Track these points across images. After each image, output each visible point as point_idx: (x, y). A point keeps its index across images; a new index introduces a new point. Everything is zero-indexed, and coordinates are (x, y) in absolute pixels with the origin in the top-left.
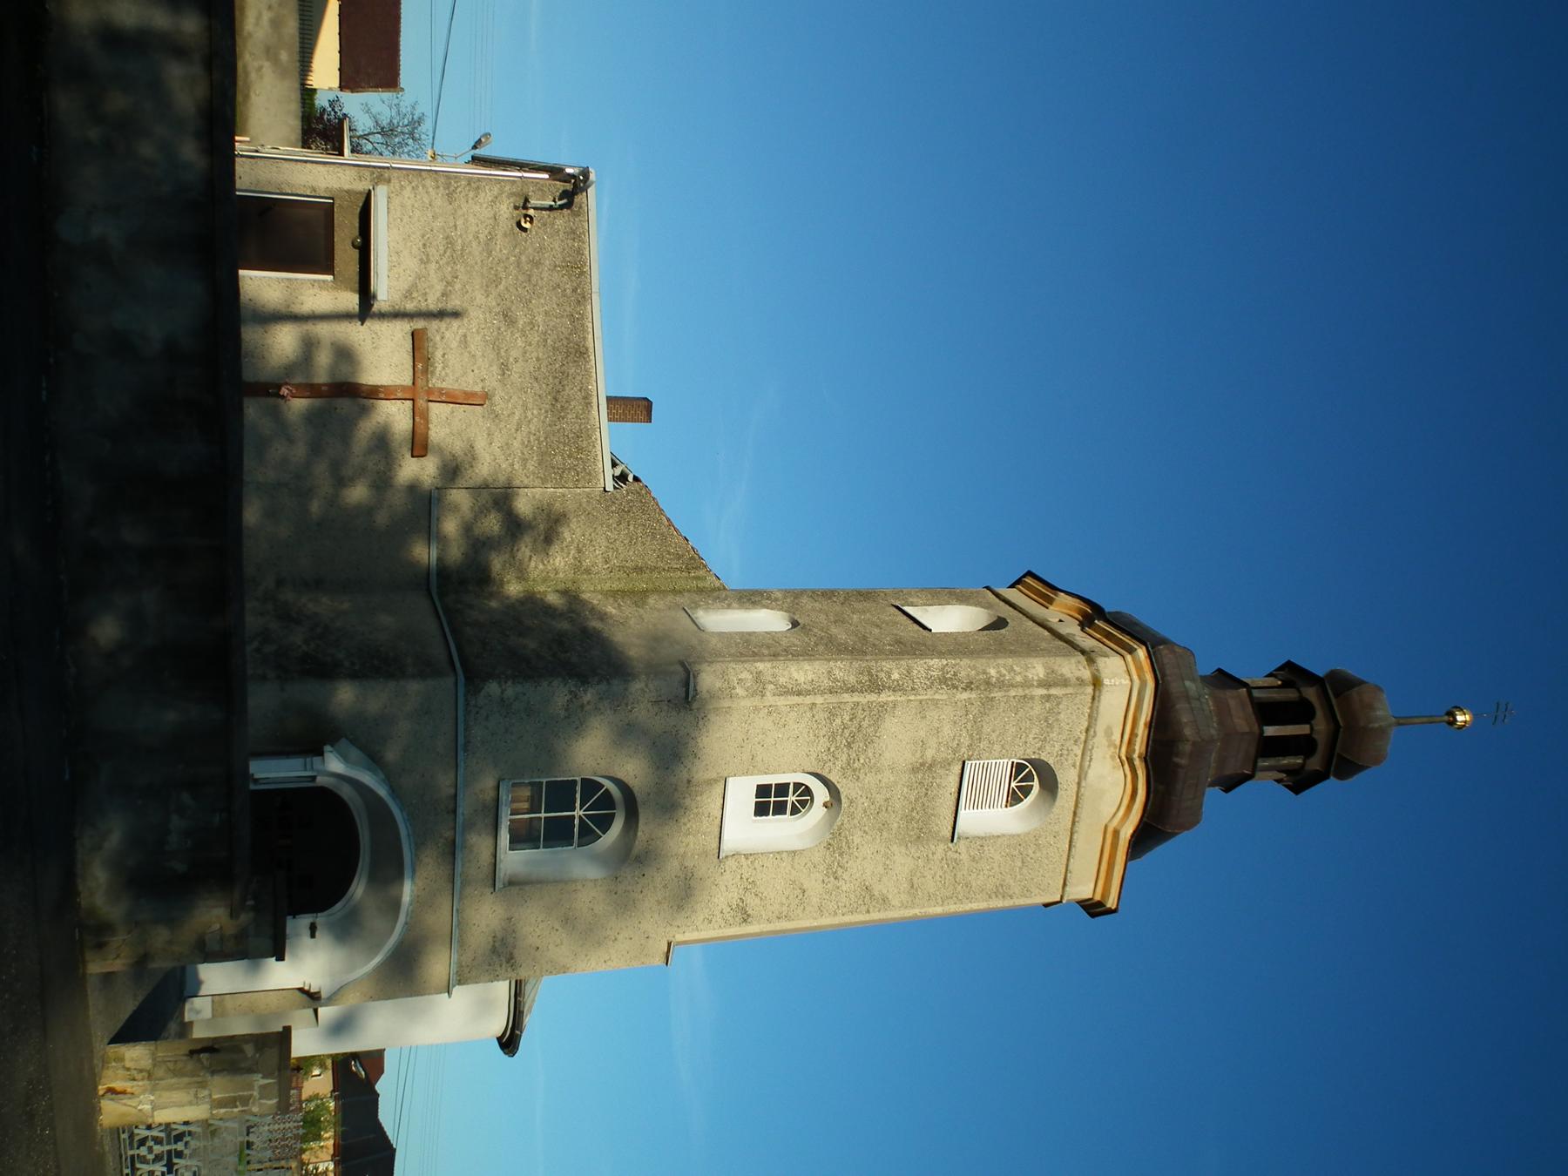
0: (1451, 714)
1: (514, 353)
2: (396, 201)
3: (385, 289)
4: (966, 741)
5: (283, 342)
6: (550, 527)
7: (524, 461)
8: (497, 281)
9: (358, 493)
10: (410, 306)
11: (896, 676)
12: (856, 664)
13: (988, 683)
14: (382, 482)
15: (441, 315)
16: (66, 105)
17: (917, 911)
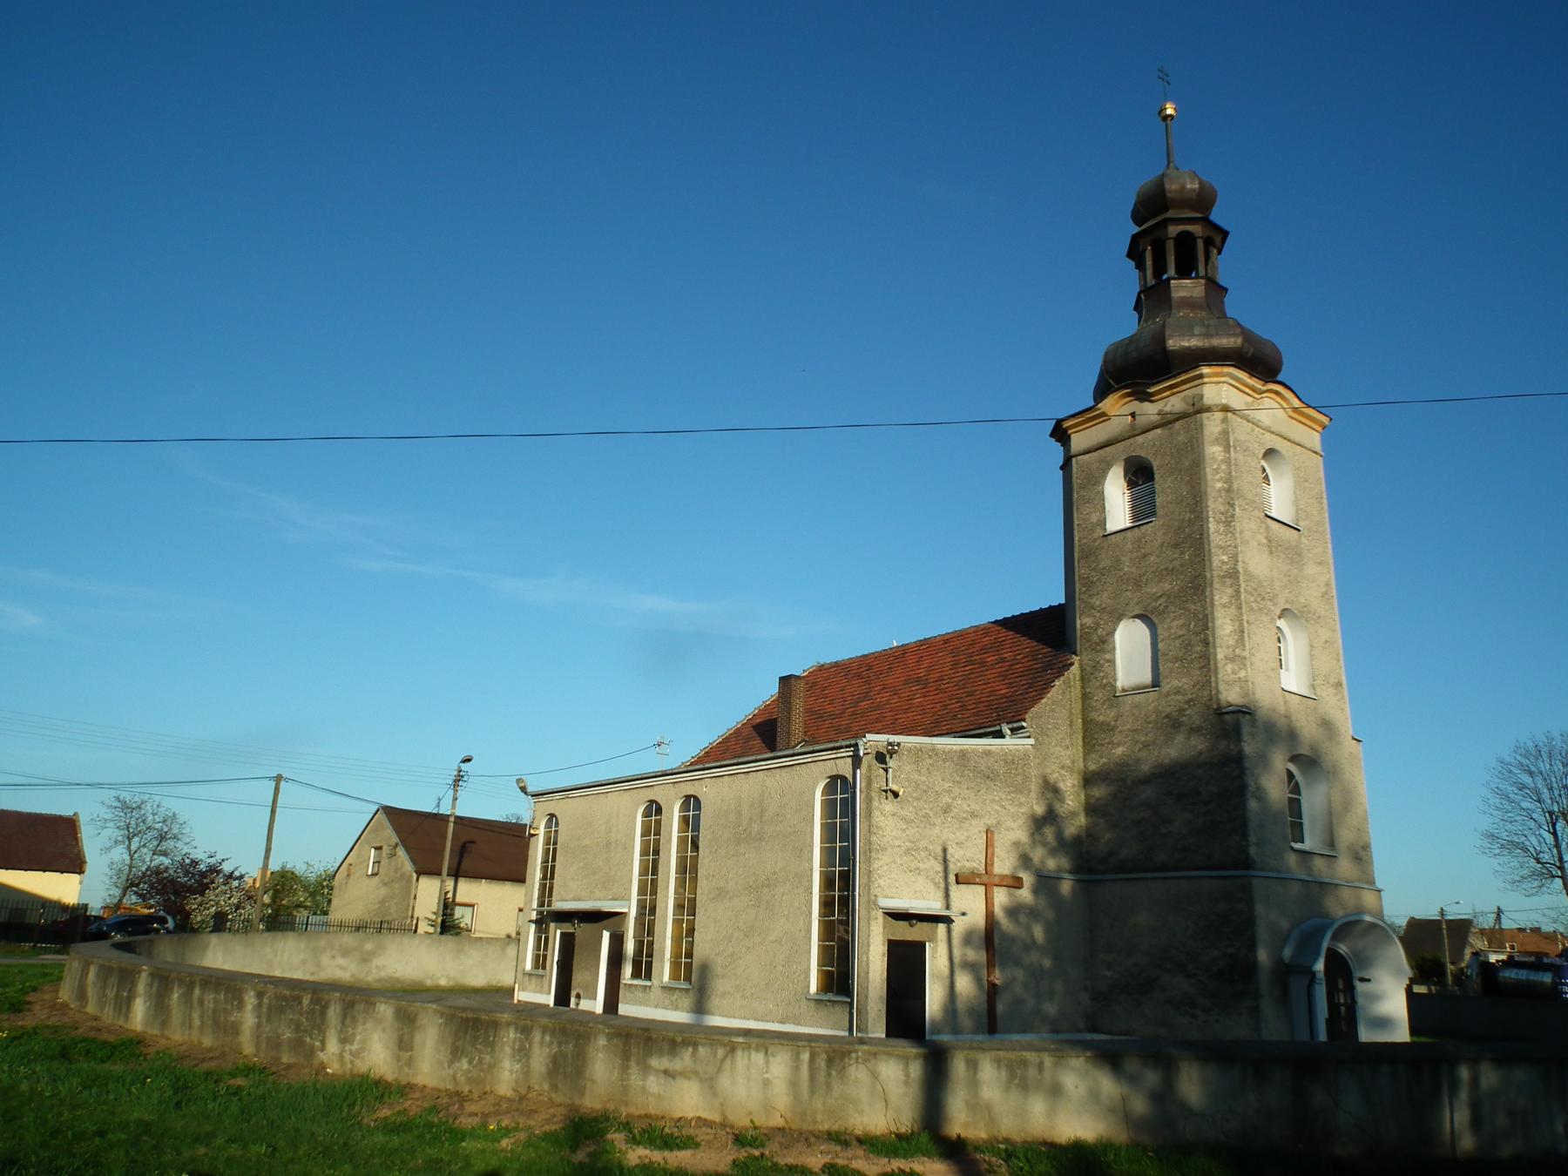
0: (1166, 118)
1: (966, 808)
2: (887, 892)
3: (934, 906)
4: (1256, 513)
5: (964, 983)
6: (1050, 789)
7: (1021, 804)
8: (926, 816)
9: (1038, 932)
10: (942, 885)
11: (1225, 558)
12: (1216, 586)
13: (1229, 491)
14: (1033, 913)
15: (945, 861)
16: (1506, 1150)
17: (1331, 561)
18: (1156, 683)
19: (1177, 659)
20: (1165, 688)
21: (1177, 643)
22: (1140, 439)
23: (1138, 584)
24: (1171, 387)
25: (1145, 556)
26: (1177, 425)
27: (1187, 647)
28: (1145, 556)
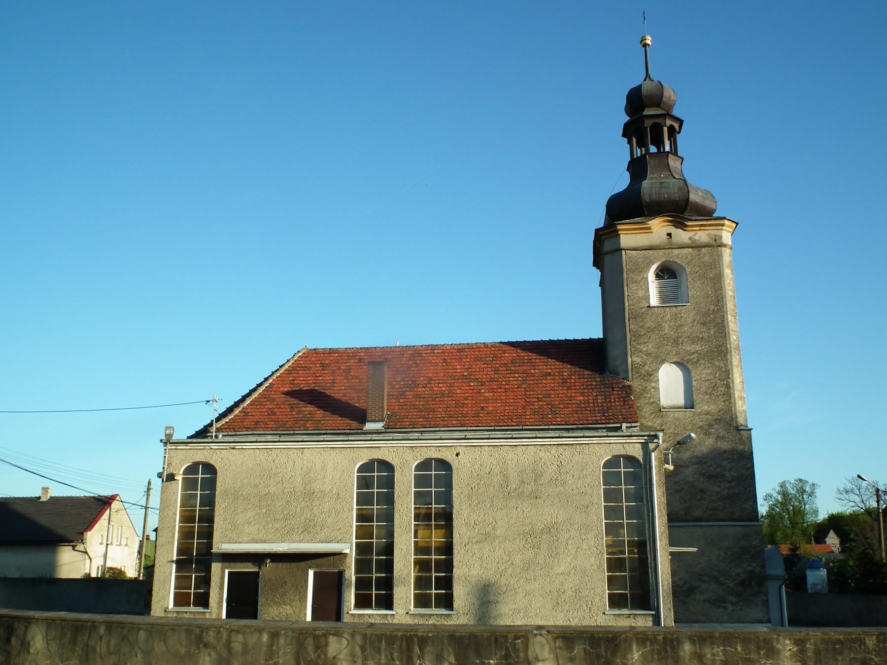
0: (645, 45)
18: (690, 405)
19: (706, 393)
20: (698, 409)
21: (707, 384)
22: (676, 252)
23: (676, 342)
24: (701, 225)
25: (681, 326)
26: (704, 250)
27: (714, 387)
28: (681, 326)
